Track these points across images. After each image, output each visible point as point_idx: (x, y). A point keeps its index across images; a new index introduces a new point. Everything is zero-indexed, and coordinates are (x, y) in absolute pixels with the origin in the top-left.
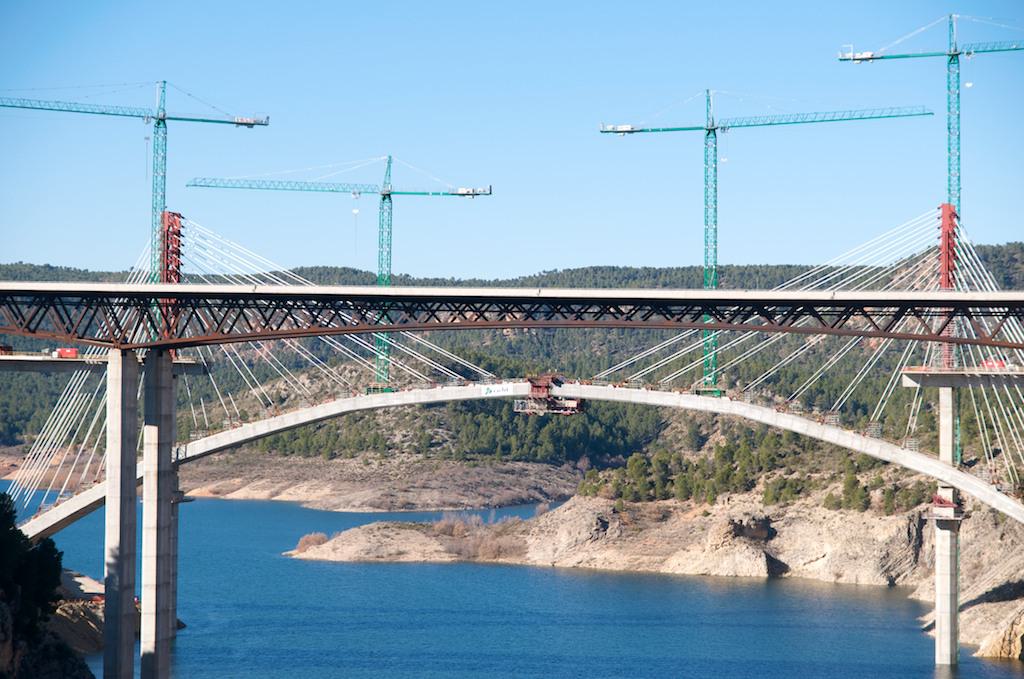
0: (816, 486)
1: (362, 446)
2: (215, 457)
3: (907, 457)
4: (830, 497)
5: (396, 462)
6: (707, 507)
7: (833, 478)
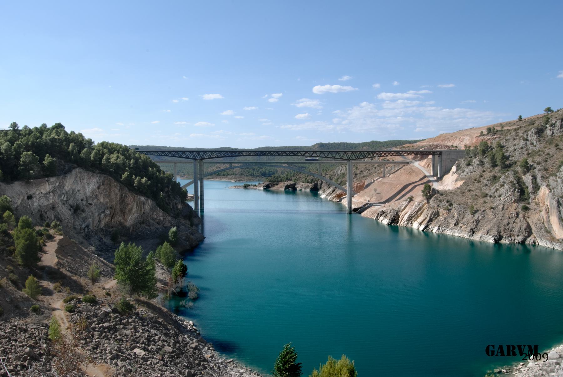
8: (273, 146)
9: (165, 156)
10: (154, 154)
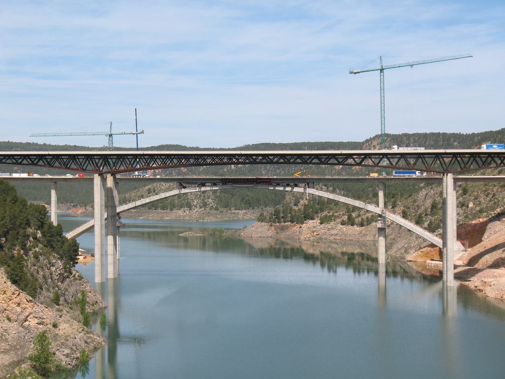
0: (338, 217)
1: (181, 206)
2: (133, 211)
3: (371, 208)
4: (343, 221)
5: (195, 211)
6: (300, 225)
7: (343, 215)
8: (277, 142)
9: (13, 163)
10: (4, 161)
